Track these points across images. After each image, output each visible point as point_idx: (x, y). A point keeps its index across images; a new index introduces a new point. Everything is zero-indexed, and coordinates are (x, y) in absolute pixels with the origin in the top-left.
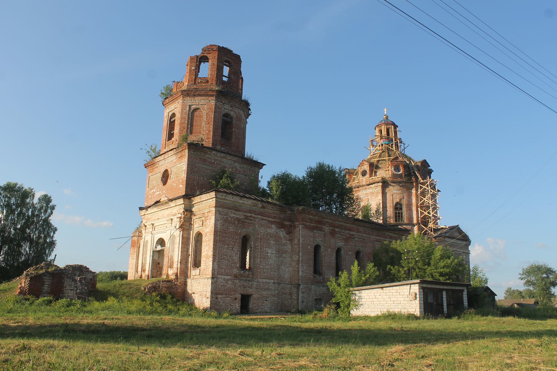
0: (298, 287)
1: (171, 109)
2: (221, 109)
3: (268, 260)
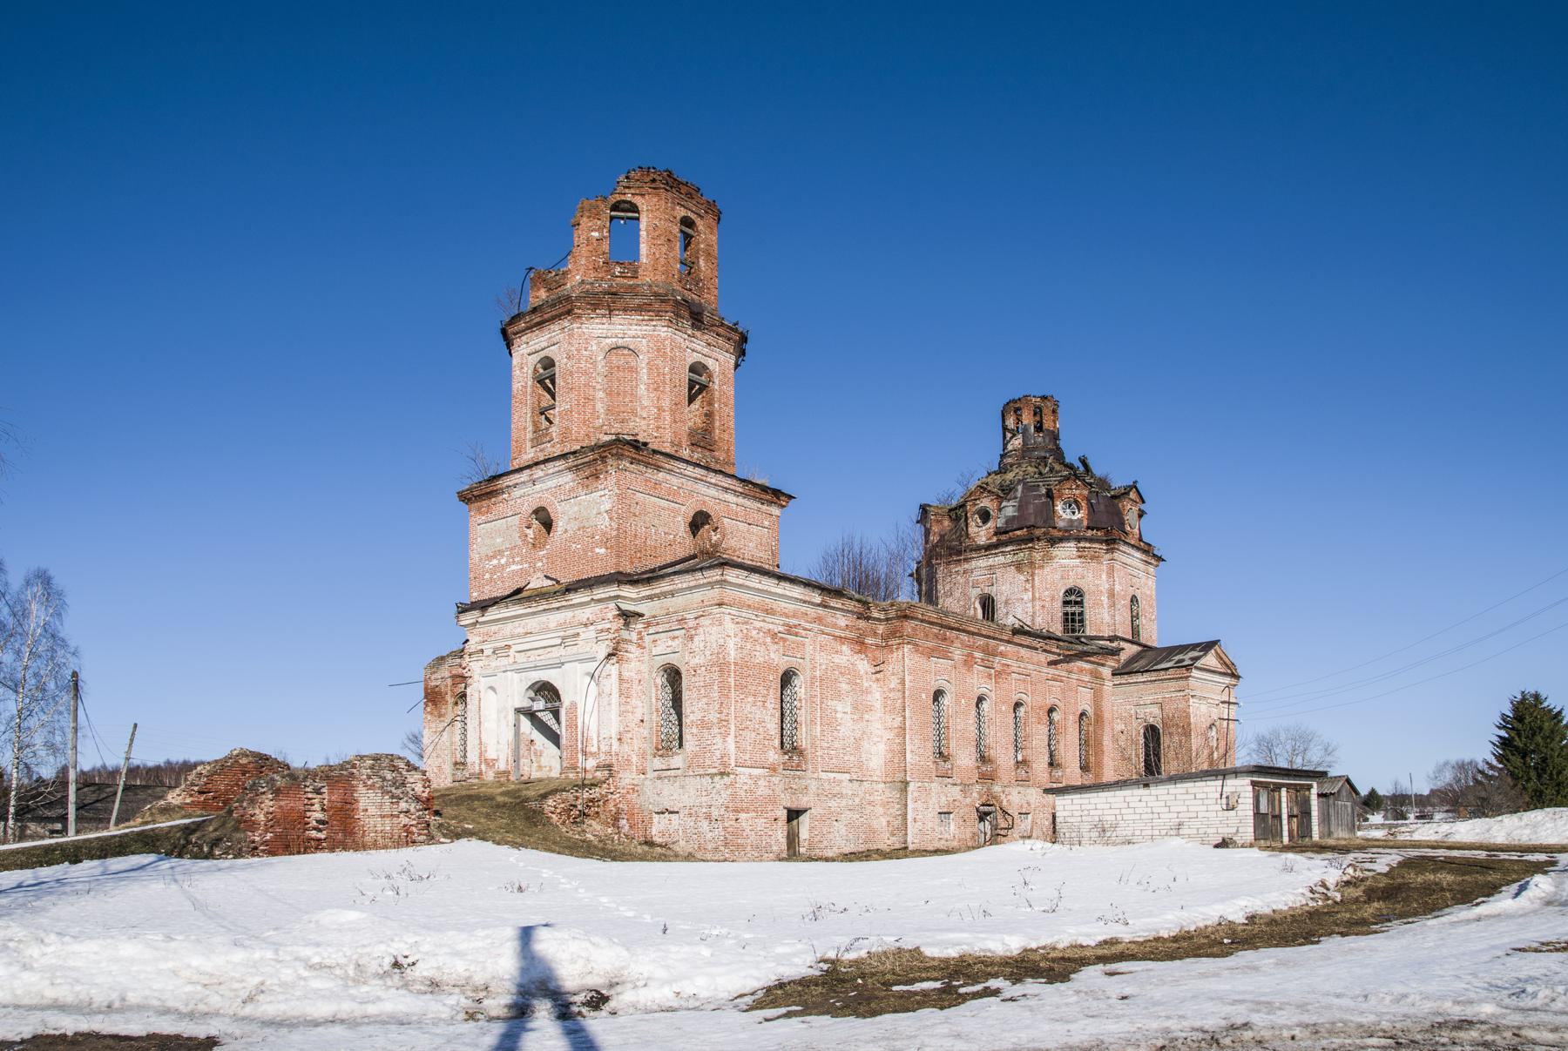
0: (906, 787)
1: (537, 347)
2: (685, 350)
3: (838, 728)
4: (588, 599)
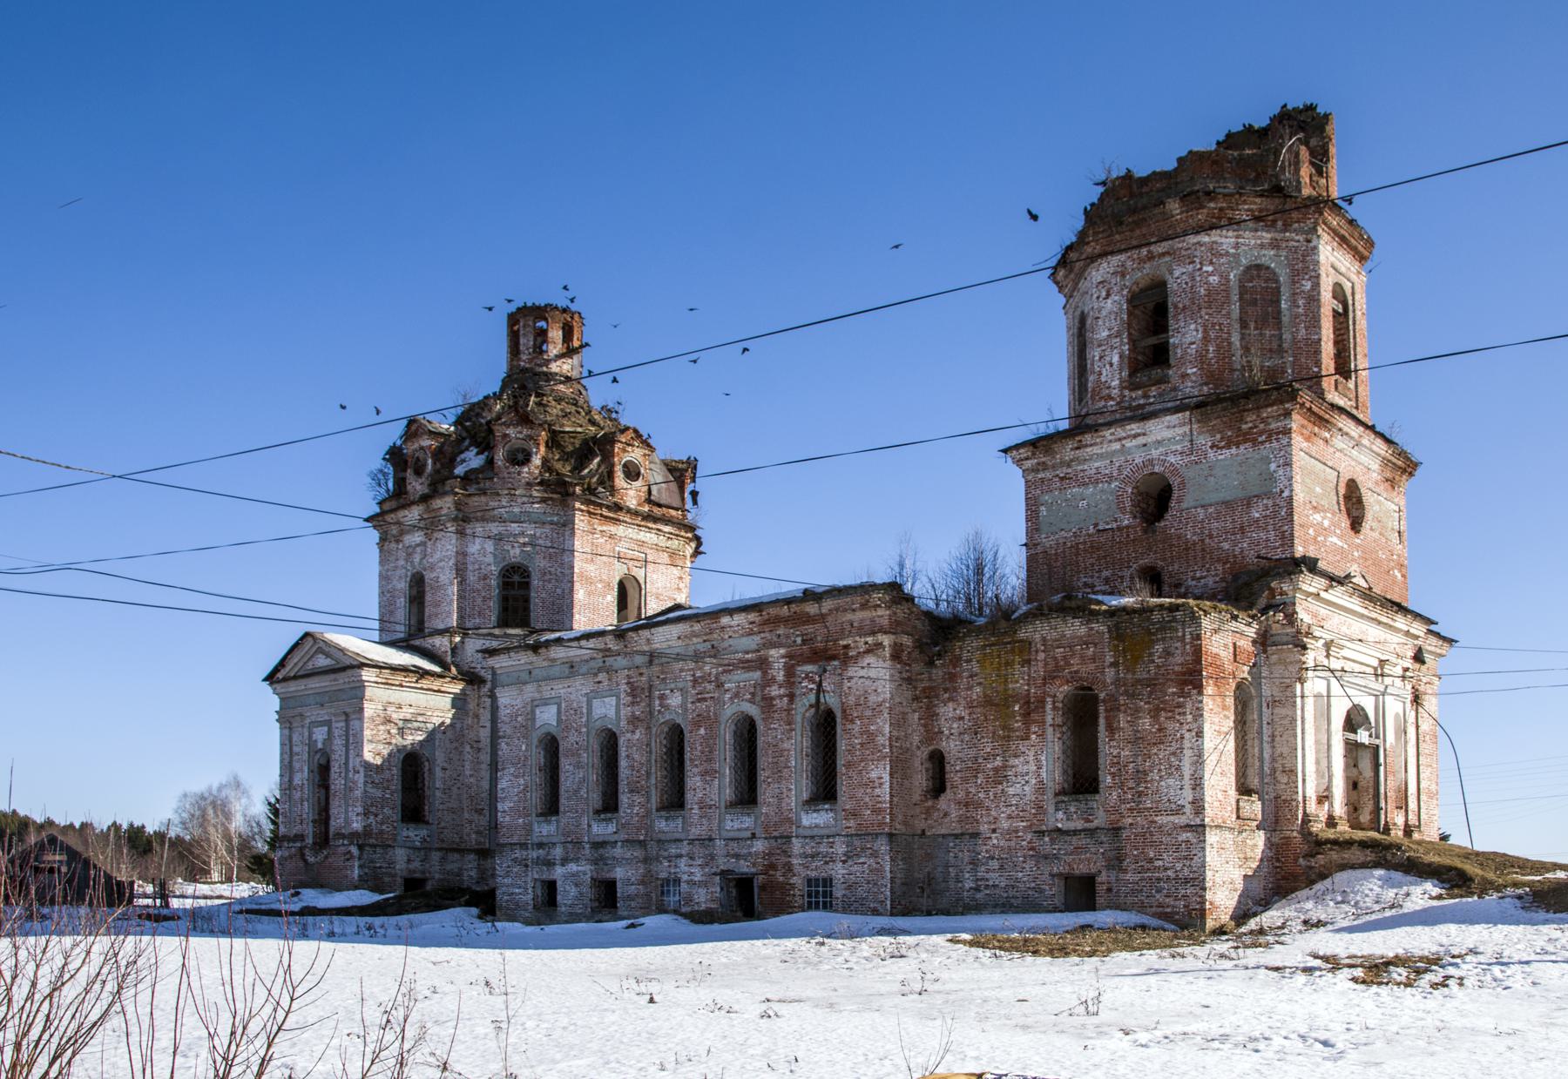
4: (1406, 628)
